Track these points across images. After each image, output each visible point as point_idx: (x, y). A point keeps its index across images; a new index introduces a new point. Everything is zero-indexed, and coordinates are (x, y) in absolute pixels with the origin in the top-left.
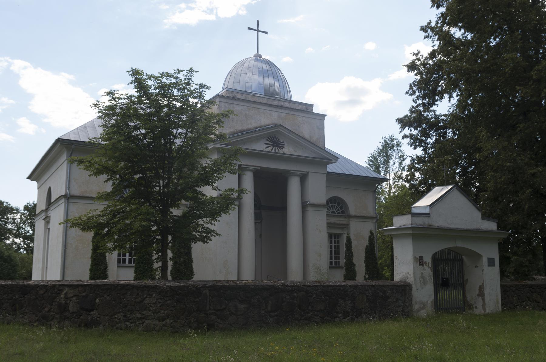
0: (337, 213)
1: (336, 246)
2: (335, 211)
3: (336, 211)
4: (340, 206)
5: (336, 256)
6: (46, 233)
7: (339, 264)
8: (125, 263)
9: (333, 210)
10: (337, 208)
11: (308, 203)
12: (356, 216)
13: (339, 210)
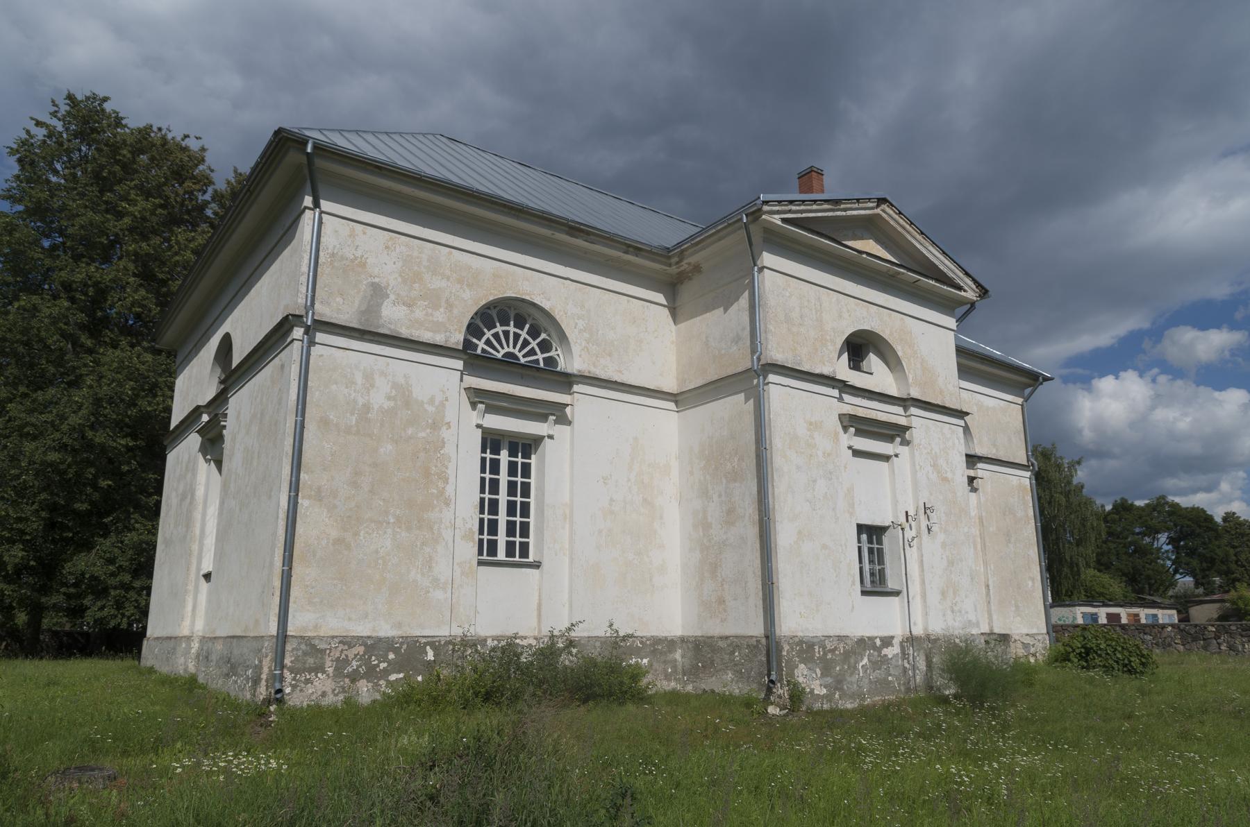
3: (520, 351)
8: (528, 558)
10: (517, 336)
11: (135, 271)
12: (318, 258)
13: (526, 343)
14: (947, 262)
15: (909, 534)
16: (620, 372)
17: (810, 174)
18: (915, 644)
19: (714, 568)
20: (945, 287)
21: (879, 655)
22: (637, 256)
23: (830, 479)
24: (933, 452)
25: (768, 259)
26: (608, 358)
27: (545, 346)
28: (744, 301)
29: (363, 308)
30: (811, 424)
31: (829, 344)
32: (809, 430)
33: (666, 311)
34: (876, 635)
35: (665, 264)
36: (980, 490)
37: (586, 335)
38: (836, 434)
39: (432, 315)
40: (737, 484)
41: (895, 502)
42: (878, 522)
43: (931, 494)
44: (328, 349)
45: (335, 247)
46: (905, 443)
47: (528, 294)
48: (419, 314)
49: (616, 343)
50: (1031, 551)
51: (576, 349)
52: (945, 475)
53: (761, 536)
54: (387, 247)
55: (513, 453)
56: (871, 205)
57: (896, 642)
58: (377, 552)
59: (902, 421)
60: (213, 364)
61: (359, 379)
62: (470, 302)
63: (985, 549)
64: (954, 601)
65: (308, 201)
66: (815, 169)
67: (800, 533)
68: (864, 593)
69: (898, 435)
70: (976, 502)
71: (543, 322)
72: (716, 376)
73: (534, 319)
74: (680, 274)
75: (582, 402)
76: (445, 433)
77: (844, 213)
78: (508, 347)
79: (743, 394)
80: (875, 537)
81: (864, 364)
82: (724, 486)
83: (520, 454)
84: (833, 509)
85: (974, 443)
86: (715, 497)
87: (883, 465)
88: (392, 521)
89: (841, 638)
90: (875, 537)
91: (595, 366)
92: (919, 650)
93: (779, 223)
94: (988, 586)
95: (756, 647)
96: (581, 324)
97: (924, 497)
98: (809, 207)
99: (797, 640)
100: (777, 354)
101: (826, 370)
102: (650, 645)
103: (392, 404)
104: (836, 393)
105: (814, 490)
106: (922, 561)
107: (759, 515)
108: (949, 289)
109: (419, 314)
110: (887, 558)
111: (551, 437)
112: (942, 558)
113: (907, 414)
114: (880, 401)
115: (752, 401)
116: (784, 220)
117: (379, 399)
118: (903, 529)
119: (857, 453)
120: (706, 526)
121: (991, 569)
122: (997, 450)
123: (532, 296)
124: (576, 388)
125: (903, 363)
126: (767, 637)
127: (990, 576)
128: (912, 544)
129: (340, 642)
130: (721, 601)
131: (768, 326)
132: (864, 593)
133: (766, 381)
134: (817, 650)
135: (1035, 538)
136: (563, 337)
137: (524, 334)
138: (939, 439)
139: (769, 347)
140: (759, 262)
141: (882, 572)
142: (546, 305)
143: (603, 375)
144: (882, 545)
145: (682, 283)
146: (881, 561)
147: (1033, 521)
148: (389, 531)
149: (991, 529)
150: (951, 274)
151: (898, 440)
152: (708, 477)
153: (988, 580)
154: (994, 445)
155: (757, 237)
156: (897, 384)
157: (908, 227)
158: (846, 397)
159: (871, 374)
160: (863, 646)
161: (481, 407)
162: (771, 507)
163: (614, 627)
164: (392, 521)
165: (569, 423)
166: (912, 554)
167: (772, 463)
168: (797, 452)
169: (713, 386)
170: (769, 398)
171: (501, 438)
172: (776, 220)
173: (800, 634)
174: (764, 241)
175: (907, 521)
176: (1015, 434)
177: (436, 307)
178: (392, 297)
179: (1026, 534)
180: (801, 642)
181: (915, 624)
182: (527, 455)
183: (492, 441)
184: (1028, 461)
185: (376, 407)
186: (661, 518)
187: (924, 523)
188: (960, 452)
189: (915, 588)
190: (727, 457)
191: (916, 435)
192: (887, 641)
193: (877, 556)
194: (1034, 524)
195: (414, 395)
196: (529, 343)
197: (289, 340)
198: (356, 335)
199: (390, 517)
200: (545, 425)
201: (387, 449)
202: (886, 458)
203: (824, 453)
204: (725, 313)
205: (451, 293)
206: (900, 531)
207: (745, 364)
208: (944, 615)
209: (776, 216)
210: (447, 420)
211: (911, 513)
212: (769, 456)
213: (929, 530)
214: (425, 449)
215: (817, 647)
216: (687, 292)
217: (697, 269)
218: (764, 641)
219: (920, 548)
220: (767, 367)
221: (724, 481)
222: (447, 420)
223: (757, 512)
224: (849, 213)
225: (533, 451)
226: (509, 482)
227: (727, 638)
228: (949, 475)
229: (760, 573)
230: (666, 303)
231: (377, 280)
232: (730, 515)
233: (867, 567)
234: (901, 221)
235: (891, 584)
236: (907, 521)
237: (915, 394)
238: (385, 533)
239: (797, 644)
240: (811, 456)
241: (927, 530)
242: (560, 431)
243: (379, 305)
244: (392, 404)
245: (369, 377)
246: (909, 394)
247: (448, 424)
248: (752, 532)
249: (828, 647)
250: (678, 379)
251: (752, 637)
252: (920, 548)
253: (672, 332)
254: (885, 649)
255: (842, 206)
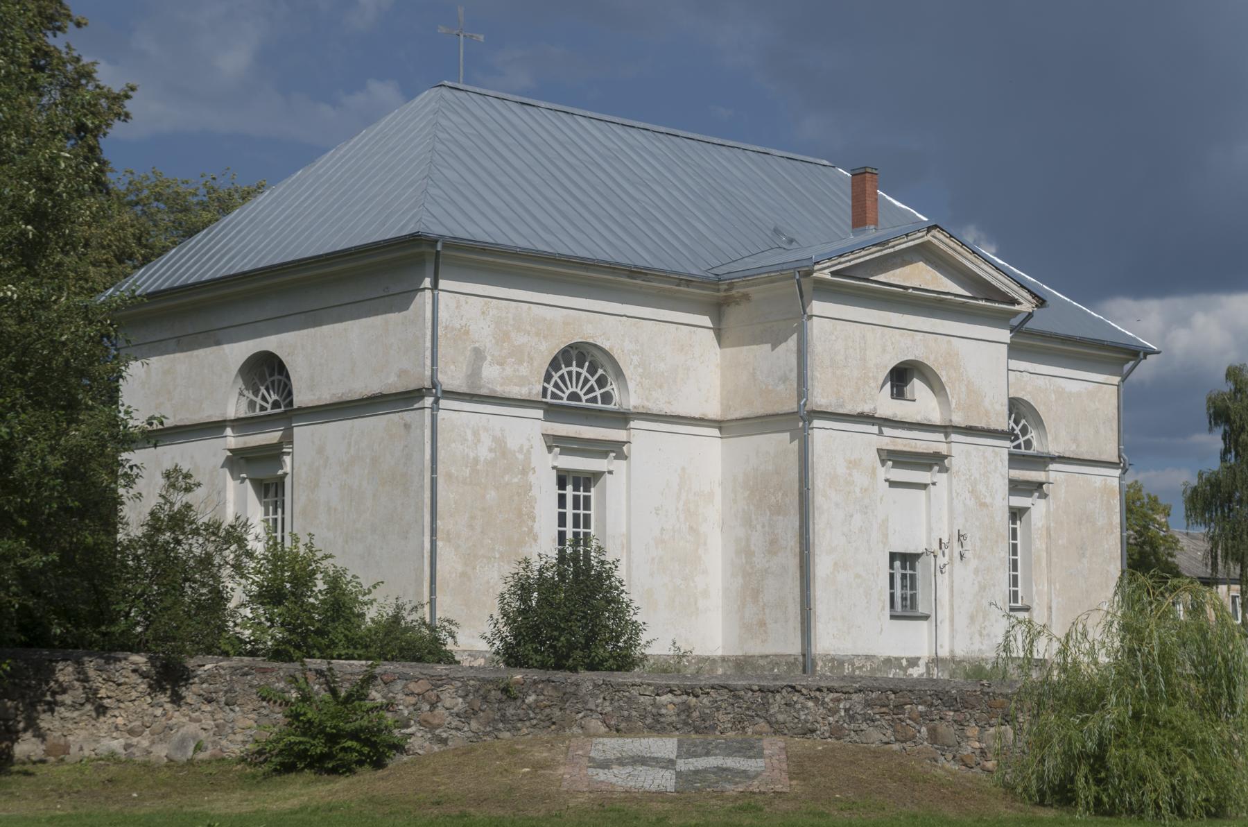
0: (587, 401)
1: (578, 515)
2: (581, 393)
3: (585, 394)
4: (596, 376)
5: (579, 515)
6: (230, 248)
7: (913, 605)
9: (574, 389)
14: (1000, 277)
15: (942, 561)
16: (669, 403)
17: (863, 176)
18: (939, 665)
19: (756, 594)
20: (997, 305)
21: (905, 674)
22: (688, 287)
23: (866, 513)
24: (973, 478)
25: (817, 307)
26: (659, 390)
27: (602, 382)
28: (792, 342)
29: (469, 373)
30: (850, 462)
31: (871, 381)
32: (848, 468)
33: (711, 333)
34: (903, 655)
35: (714, 290)
36: (1051, 496)
37: (640, 370)
38: (874, 470)
39: (518, 370)
40: (781, 518)
41: (930, 530)
42: (911, 550)
43: (967, 521)
44: (454, 415)
45: (447, 320)
46: (944, 470)
47: (592, 337)
48: (509, 371)
49: (666, 374)
50: (1112, 566)
51: (631, 385)
52: (983, 500)
53: (801, 567)
54: (483, 313)
55: (576, 488)
56: (920, 234)
57: (922, 663)
58: (488, 582)
59: (943, 448)
60: (236, 376)
61: (470, 437)
62: (548, 349)
63: (1050, 566)
64: (983, 625)
65: (427, 282)
66: (869, 170)
67: (836, 564)
68: (893, 617)
69: (936, 464)
70: (1044, 510)
71: (600, 357)
72: (763, 410)
73: (592, 356)
74: (727, 297)
75: (640, 437)
76: (532, 478)
77: (892, 250)
78: (581, 390)
79: (788, 434)
80: (908, 563)
81: (908, 389)
82: (768, 518)
83: (582, 488)
84: (868, 541)
85: (1047, 439)
86: (759, 527)
87: (922, 493)
88: (497, 556)
89: (868, 657)
90: (908, 563)
91: (648, 400)
92: (943, 671)
93: (829, 277)
94: (1050, 608)
95: (794, 664)
96: (636, 359)
97: (959, 524)
98: (858, 255)
99: (830, 657)
100: (821, 398)
101: (866, 408)
102: (695, 663)
103: (493, 455)
104: (875, 429)
105: (850, 524)
106: (953, 587)
107: (800, 548)
108: (1001, 306)
109: (509, 371)
110: (919, 584)
111: (610, 472)
112: (973, 584)
113: (948, 440)
114: (920, 430)
115: (796, 442)
116: (833, 274)
117: (484, 452)
118: (935, 556)
119: (893, 484)
120: (749, 554)
121: (1055, 589)
122: (1078, 446)
123: (595, 339)
124: (633, 424)
125: (947, 388)
126: (804, 655)
127: (1053, 596)
128: (944, 570)
129: (469, 655)
130: (762, 624)
131: (814, 373)
132: (893, 617)
133: (811, 426)
134: (846, 667)
135: (1119, 551)
136: (619, 374)
137: (584, 372)
138: (981, 463)
139: (815, 393)
140: (808, 310)
141: (913, 597)
142: (606, 345)
143: (655, 409)
144: (915, 571)
145: (728, 306)
146: (913, 587)
147: (1119, 530)
148: (496, 564)
149: (1060, 542)
150: (1004, 289)
151: (936, 468)
152: (752, 507)
153: (1051, 601)
154: (1075, 440)
155: (807, 285)
156: (940, 408)
157: (959, 248)
158: (886, 431)
159: (914, 401)
160: (889, 665)
161: (557, 450)
162: (811, 541)
163: (676, 645)
164: (497, 556)
165: (626, 458)
166: (943, 581)
167: (813, 502)
168: (836, 490)
169: (760, 420)
170: (813, 442)
171: (566, 474)
172: (826, 275)
173: (832, 653)
174: (814, 290)
175: (941, 548)
176: (1104, 423)
177: (520, 362)
178: (489, 358)
179: (1106, 546)
180: (833, 660)
181: (941, 646)
182: (587, 489)
183: (563, 479)
184: (1120, 457)
185: (482, 459)
186: (705, 544)
187: (957, 549)
188: (1002, 476)
189: (944, 613)
190: (772, 490)
191: (956, 463)
192: (913, 662)
193: (910, 582)
194: (1119, 534)
195: (509, 445)
196: (588, 381)
197: (416, 406)
198: (467, 398)
199: (496, 553)
200: (605, 461)
201: (492, 495)
202: (924, 486)
203: (861, 489)
204: (773, 350)
205: (531, 347)
206: (933, 558)
207: (791, 406)
208: (971, 638)
209: (827, 271)
210: (532, 466)
211: (945, 540)
212: (811, 495)
213: (962, 556)
214: (518, 493)
215: (846, 665)
216: (734, 315)
217: (746, 297)
218: (801, 659)
219: (951, 575)
220: (812, 415)
221: (768, 514)
222: (532, 466)
223: (798, 545)
224: (897, 248)
225: (592, 485)
226: (574, 515)
227: (767, 656)
228: (988, 500)
229: (799, 600)
230: (712, 326)
231: (477, 345)
232: (773, 545)
233: (898, 592)
234: (952, 244)
235: (921, 609)
236: (941, 548)
237: (958, 419)
238: (493, 566)
239: (830, 661)
240: (849, 493)
241: (959, 557)
242: (618, 466)
243: (480, 368)
244: (493, 455)
245: (476, 433)
246: (951, 421)
247: (534, 469)
248: (793, 563)
249: (857, 664)
250: (722, 404)
251: (790, 655)
252: (951, 575)
253: (716, 354)
254: (911, 669)
255: (890, 244)
